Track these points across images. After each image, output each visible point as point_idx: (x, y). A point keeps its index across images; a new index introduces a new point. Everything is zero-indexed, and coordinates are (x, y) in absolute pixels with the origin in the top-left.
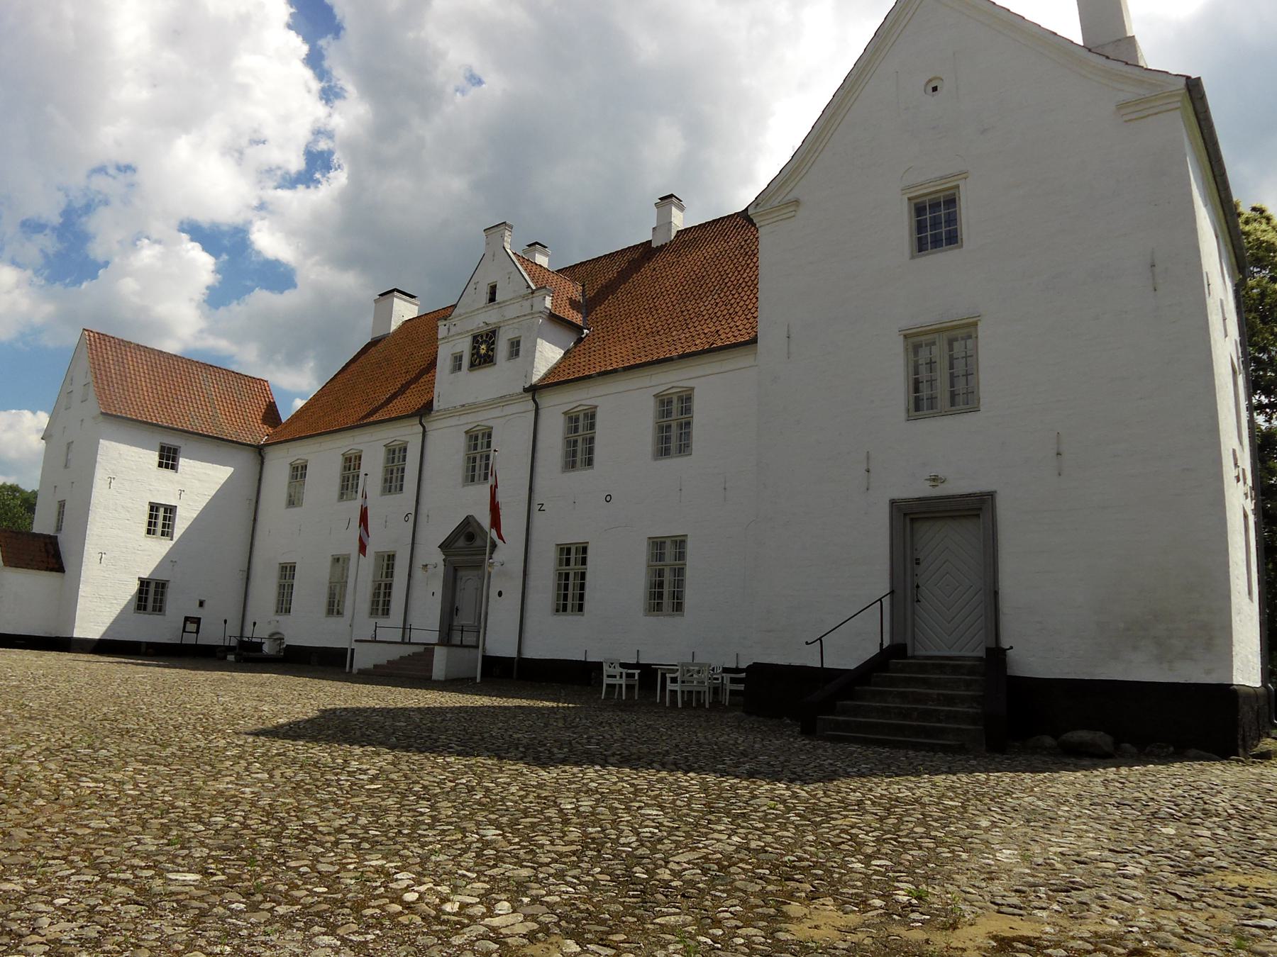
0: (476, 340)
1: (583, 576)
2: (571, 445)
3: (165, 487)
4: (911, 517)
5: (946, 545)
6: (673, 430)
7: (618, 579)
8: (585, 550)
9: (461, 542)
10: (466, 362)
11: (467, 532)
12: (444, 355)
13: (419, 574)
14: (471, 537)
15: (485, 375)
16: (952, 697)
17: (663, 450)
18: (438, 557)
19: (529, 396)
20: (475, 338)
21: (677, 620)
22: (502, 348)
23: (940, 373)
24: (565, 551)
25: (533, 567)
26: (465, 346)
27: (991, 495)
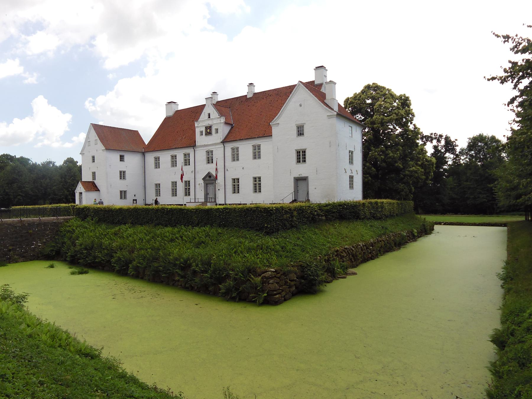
0: (207, 128)
2: (233, 155)
3: (122, 166)
5: (301, 184)
6: (257, 154)
7: (247, 185)
8: (238, 179)
9: (208, 178)
10: (204, 133)
11: (209, 175)
12: (198, 131)
13: (197, 186)
15: (209, 137)
16: (131, 397)
17: (255, 158)
18: (202, 182)
20: (206, 127)
21: (238, 162)
22: (213, 131)
23: (301, 156)
24: (234, 180)
25: (226, 183)
26: (203, 129)
27: (307, 177)
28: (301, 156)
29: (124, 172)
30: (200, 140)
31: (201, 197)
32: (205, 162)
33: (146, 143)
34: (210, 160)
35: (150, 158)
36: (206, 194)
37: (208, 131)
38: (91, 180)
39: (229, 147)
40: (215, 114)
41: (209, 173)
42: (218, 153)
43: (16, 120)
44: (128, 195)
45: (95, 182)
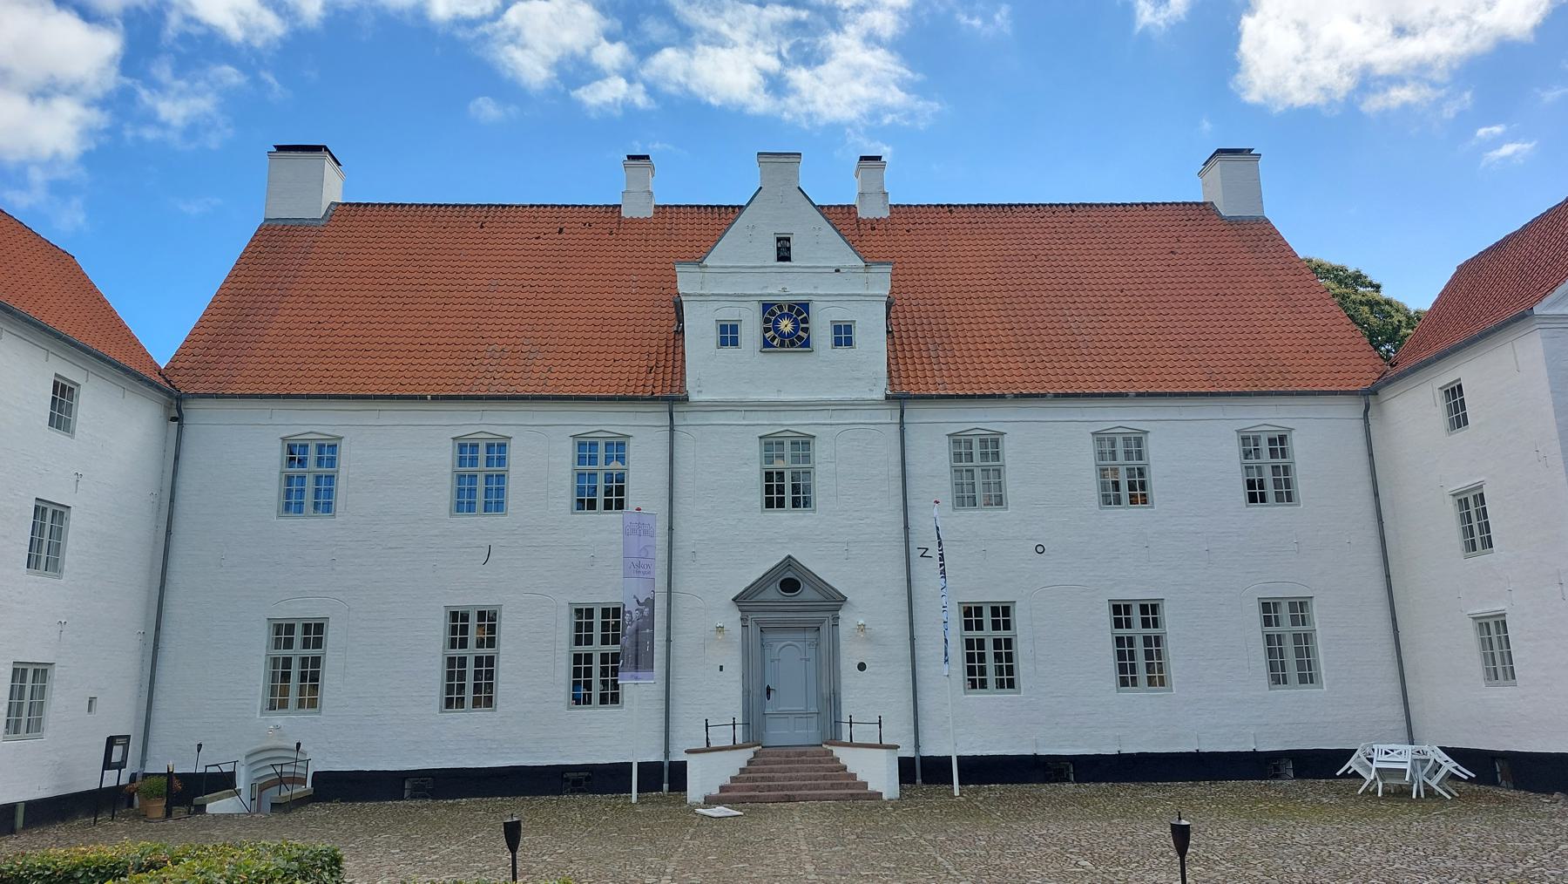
7: (534, 660)
9: (773, 593)
11: (789, 579)
12: (699, 327)
14: (790, 586)
15: (787, 362)
18: (732, 619)
19: (889, 416)
20: (766, 306)
35: (243, 446)
36: (759, 694)
37: (787, 326)
39: (935, 430)
41: (789, 562)
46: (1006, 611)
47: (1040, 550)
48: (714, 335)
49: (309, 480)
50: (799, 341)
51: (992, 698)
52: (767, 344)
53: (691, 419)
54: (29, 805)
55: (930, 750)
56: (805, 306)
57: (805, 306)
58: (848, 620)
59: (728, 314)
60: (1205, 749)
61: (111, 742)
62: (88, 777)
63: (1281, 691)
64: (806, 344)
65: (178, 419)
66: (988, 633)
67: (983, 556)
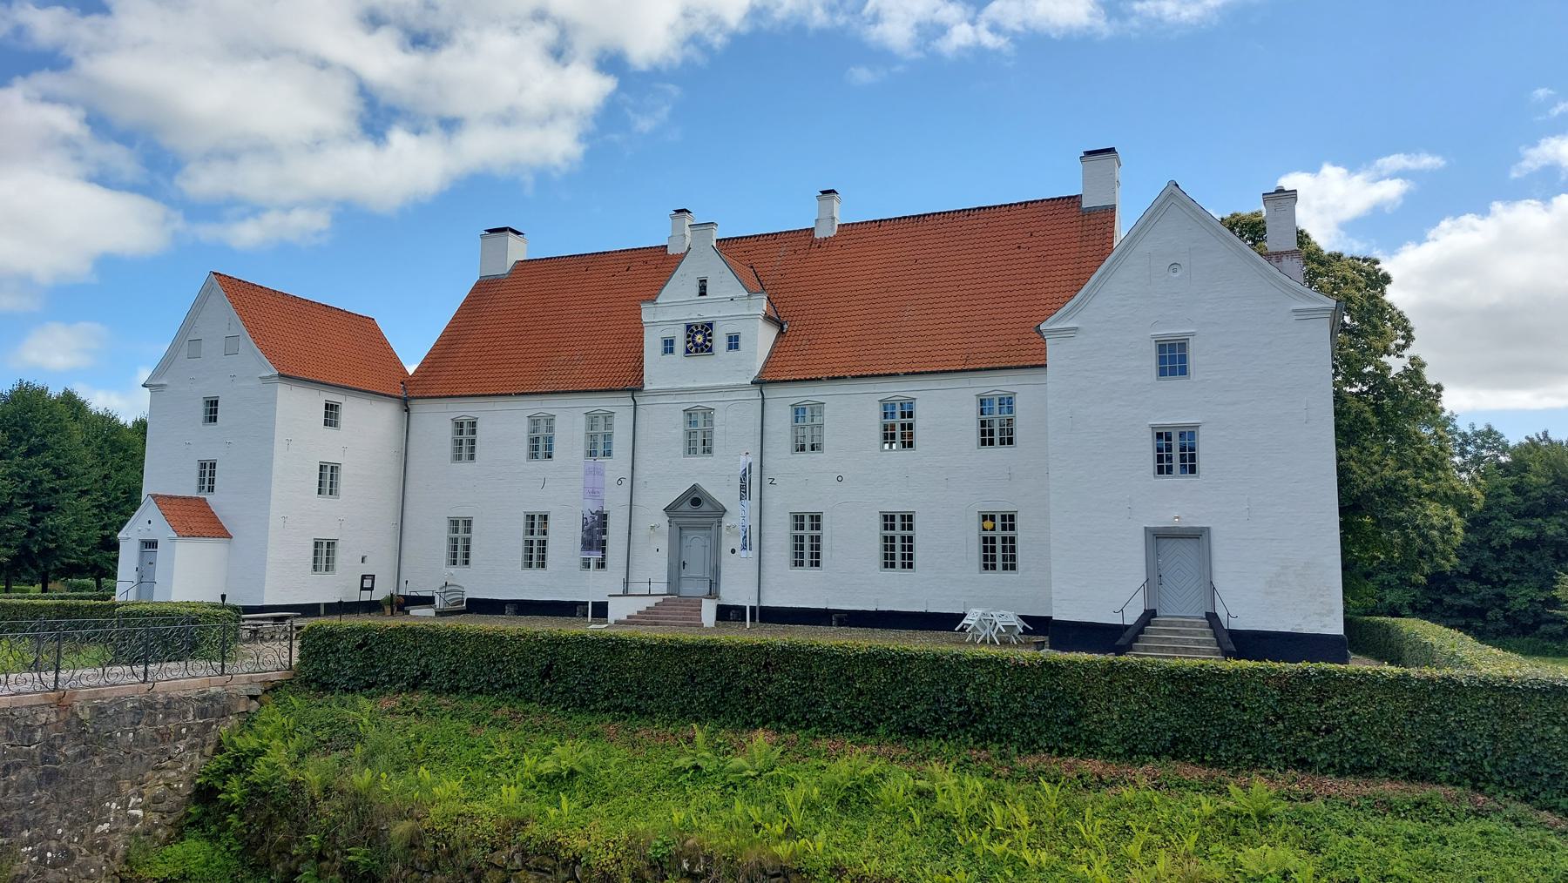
0: (691, 329)
1: (473, 442)
4: (1158, 537)
5: (1179, 555)
7: (564, 540)
9: (687, 506)
10: (680, 345)
11: (695, 498)
14: (696, 502)
15: (701, 361)
18: (663, 521)
19: (755, 393)
20: (689, 327)
28: (1175, 453)
29: (335, 468)
30: (658, 369)
31: (653, 571)
32: (680, 448)
33: (411, 370)
34: (700, 441)
35: (436, 420)
36: (678, 566)
37: (699, 339)
38: (189, 489)
39: (782, 400)
40: (725, 283)
41: (695, 488)
42: (735, 423)
43: (1497, 206)
44: (340, 556)
45: (210, 498)
46: (1012, 518)
47: (840, 479)
48: (660, 347)
49: (465, 441)
50: (706, 348)
51: (807, 572)
52: (688, 351)
53: (647, 400)
54: (326, 605)
55: (766, 603)
56: (710, 325)
57: (710, 325)
58: (727, 521)
59: (668, 334)
60: (931, 610)
61: (364, 577)
62: (354, 595)
63: (990, 574)
64: (710, 350)
65: (407, 410)
66: (999, 534)
67: (797, 484)
